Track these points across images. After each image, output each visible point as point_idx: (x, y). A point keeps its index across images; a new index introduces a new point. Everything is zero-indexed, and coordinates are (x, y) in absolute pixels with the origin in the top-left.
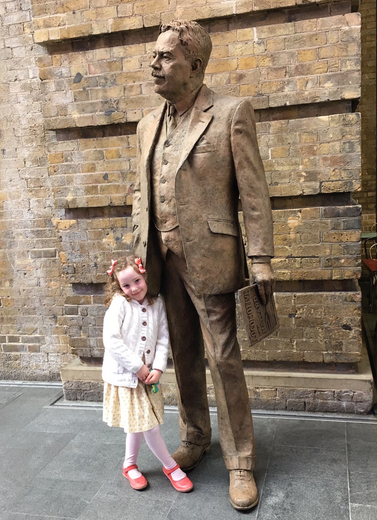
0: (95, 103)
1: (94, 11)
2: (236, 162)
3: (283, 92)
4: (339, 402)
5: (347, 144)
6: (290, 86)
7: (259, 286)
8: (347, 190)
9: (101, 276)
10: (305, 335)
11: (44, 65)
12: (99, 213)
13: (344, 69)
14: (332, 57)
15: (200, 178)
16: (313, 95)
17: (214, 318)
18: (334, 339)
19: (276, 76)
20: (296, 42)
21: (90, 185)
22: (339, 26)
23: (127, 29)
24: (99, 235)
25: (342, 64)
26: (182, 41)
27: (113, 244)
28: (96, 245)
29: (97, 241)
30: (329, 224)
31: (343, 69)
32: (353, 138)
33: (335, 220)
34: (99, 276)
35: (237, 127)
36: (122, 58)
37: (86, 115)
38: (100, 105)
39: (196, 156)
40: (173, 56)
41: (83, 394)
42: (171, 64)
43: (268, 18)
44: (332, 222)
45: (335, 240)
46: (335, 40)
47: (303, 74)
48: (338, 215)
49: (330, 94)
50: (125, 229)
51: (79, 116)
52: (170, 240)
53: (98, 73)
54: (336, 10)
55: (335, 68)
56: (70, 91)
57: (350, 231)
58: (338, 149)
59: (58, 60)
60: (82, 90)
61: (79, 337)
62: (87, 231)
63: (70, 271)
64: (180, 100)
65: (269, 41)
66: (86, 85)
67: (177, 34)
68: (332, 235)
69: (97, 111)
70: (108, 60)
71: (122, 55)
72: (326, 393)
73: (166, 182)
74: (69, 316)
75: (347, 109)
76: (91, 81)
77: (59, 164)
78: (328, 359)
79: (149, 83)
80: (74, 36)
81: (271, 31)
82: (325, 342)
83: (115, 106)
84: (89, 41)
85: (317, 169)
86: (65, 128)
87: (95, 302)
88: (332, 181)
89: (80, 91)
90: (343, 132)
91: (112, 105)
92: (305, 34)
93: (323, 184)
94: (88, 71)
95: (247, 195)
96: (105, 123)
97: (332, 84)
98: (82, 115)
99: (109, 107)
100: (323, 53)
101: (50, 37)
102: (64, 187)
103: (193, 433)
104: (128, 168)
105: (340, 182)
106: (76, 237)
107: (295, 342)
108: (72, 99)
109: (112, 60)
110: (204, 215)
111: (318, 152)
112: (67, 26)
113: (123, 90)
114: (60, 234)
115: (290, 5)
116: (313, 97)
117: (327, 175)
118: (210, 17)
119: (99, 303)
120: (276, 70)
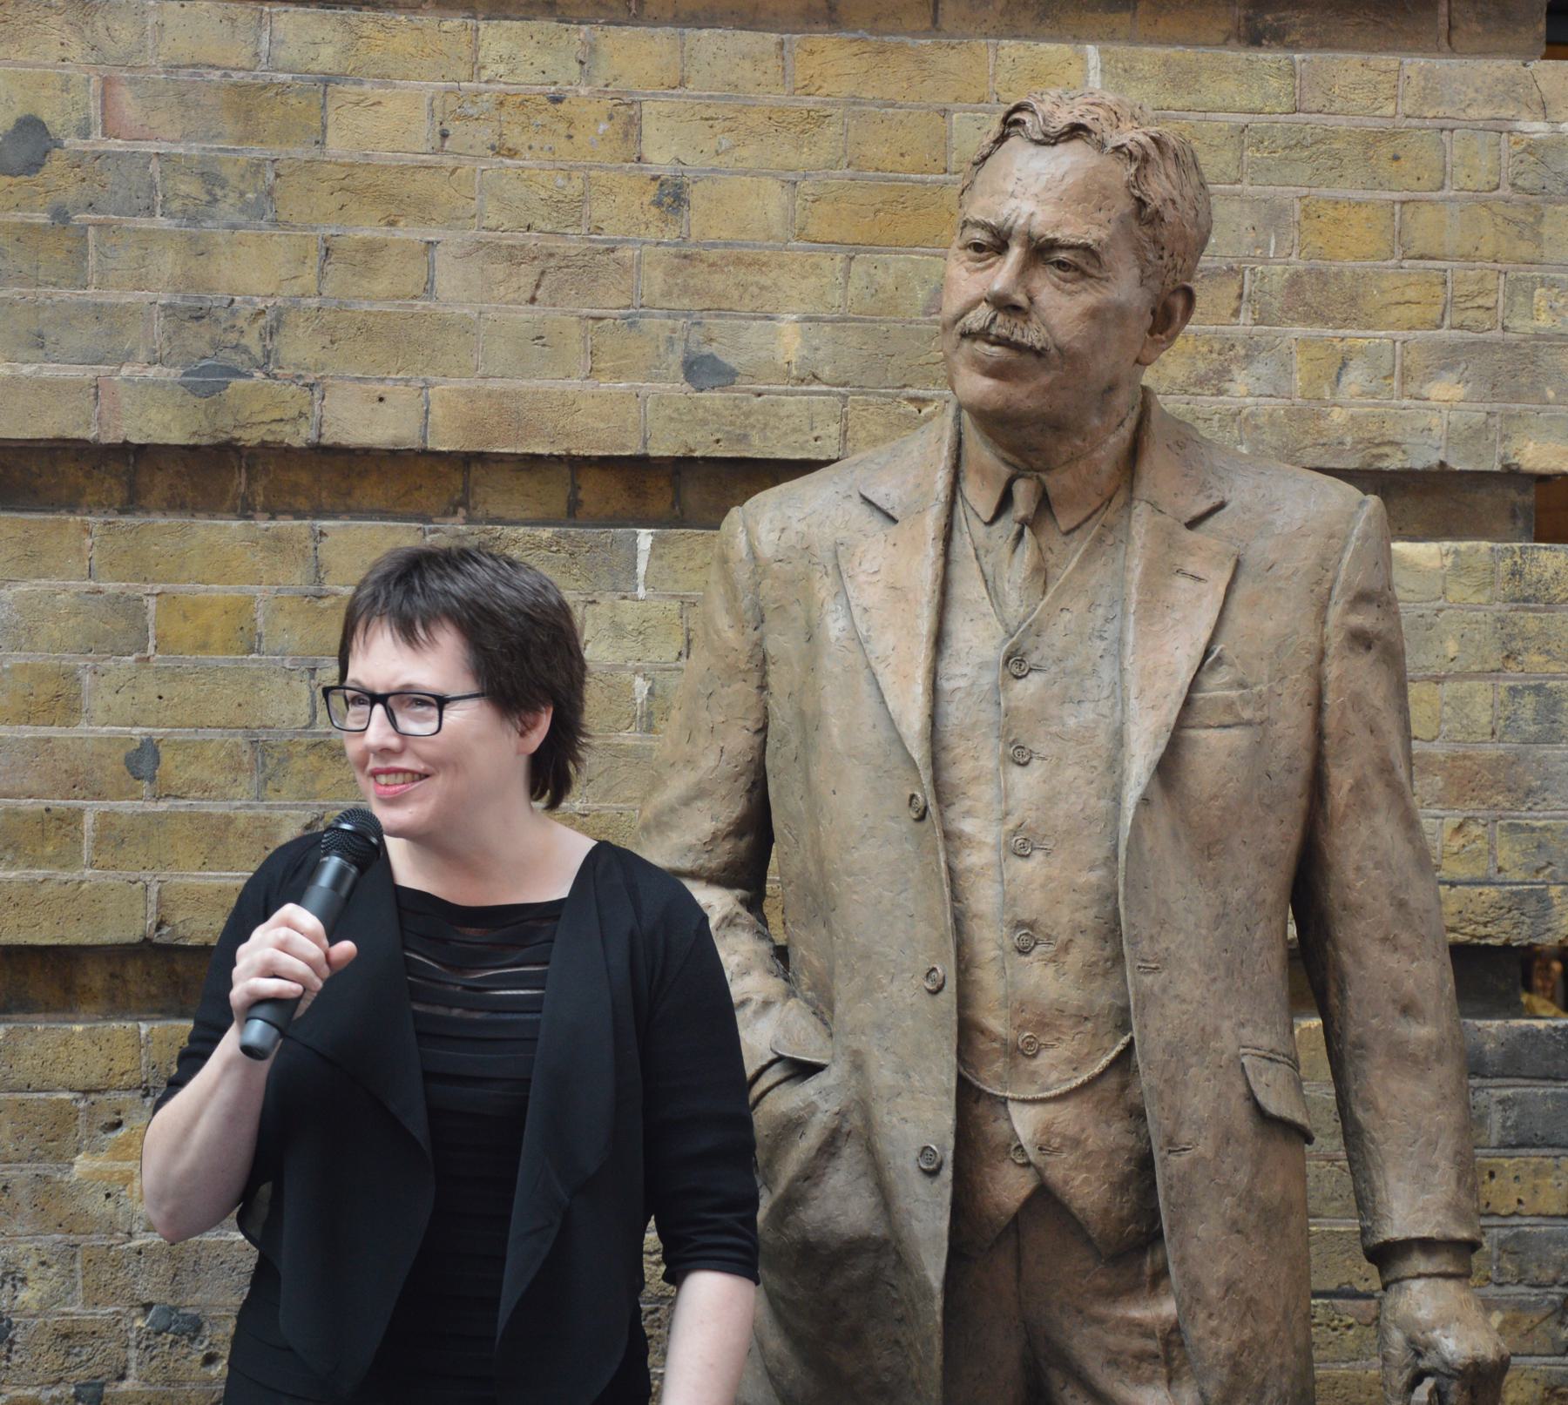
0: (125, 308)
2: (1341, 780)
3: (1220, 392)
5: (1529, 700)
6: (1260, 369)
8: (1521, 935)
13: (1522, 325)
14: (1466, 257)
15: (1208, 847)
20: (1295, 154)
21: (26, 804)
22: (1504, 113)
25: (1510, 298)
26: (1141, 203)
29: (30, 1169)
31: (1516, 323)
32: (1553, 668)
36: (327, 80)
37: (50, 371)
38: (159, 324)
46: (1481, 179)
52: (1056, 1142)
53: (169, 138)
55: (1480, 314)
57: (1534, 1156)
58: (1485, 718)
60: (41, 218)
64: (1072, 460)
69: (129, 357)
70: (236, 76)
71: (327, 59)
73: (1038, 856)
75: (1514, 516)
79: (480, 245)
83: (252, 341)
88: (1453, 884)
89: (31, 227)
90: (1511, 637)
91: (232, 337)
94: (95, 113)
95: (1385, 940)
96: (176, 437)
97: (1460, 391)
98: (27, 370)
99: (216, 345)
100: (1424, 228)
104: (304, 719)
105: (1491, 893)
110: (1226, 1025)
113: (314, 260)
116: (1371, 443)
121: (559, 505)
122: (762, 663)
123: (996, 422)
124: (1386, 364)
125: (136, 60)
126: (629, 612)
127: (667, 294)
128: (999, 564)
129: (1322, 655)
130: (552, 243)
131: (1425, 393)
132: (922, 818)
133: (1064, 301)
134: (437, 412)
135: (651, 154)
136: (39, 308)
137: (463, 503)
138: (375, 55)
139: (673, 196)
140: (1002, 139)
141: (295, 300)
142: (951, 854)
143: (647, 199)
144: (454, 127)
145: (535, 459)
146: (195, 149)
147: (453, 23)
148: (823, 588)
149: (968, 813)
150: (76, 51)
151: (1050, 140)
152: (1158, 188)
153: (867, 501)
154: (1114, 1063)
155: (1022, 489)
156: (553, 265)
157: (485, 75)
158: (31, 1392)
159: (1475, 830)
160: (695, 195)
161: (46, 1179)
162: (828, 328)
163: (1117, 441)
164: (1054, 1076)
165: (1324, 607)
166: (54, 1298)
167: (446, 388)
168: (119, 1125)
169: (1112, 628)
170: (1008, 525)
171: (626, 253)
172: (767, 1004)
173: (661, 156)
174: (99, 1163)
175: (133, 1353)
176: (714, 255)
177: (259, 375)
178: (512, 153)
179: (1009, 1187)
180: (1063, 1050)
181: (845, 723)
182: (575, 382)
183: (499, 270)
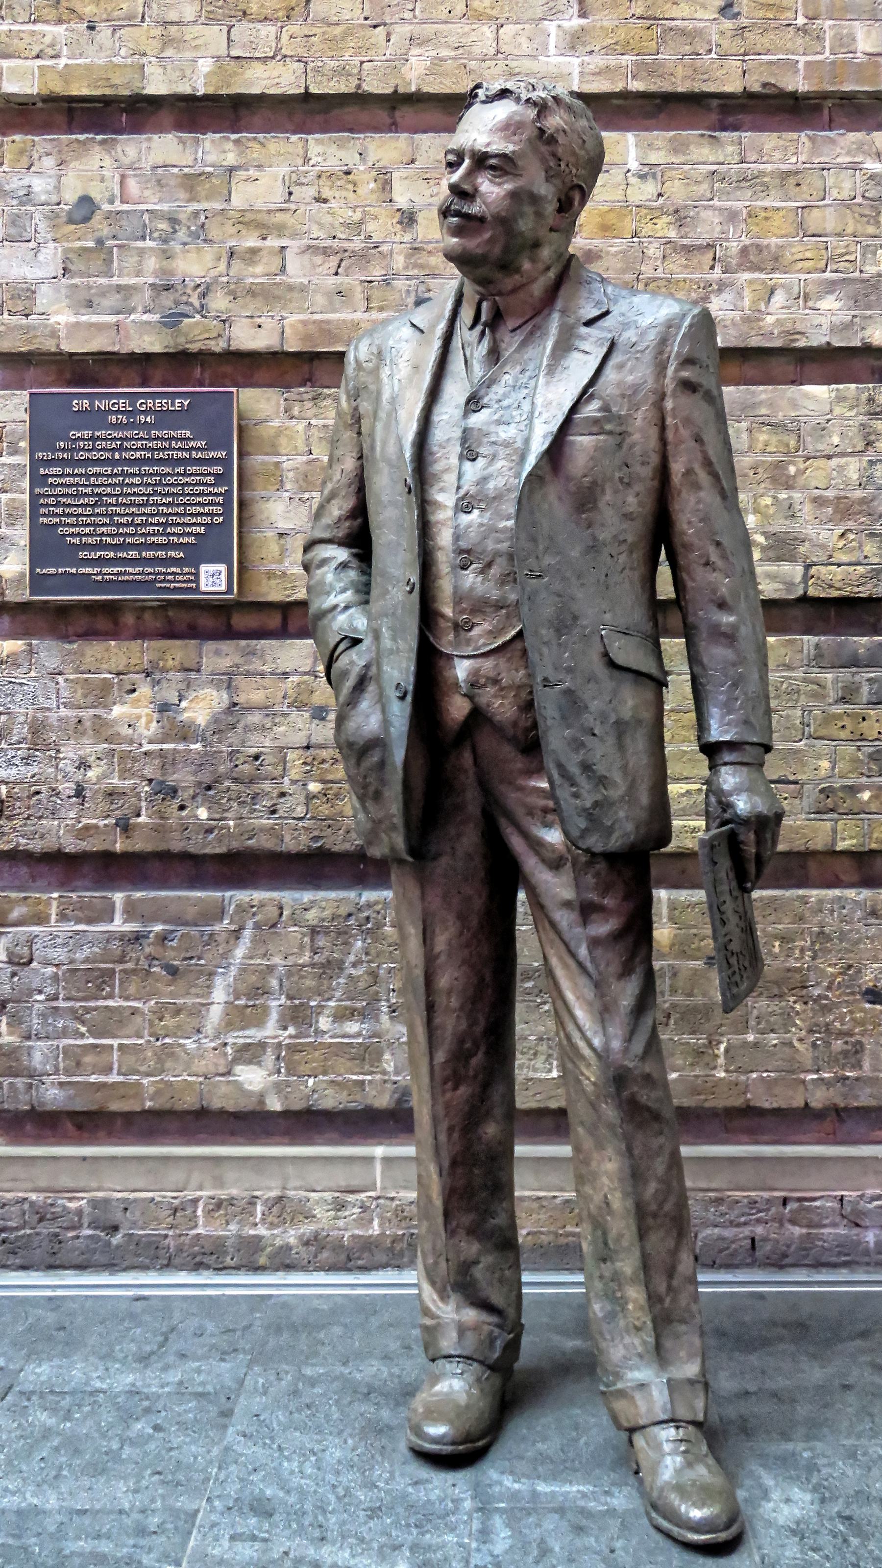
1: (157, 31)
2: (677, 468)
4: (856, 1231)
7: (741, 830)
9: (96, 827)
10: (752, 1023)
12: (102, 623)
14: (838, 235)
16: (789, 326)
17: (603, 928)
18: (841, 1034)
19: (686, 266)
20: (743, 184)
22: (856, 160)
23: (256, 90)
24: (102, 695)
25: (863, 255)
26: (542, 131)
27: (149, 722)
28: (88, 724)
29: (92, 712)
30: (829, 685)
33: (845, 674)
34: (87, 828)
35: (685, 374)
36: (231, 170)
37: (95, 319)
38: (148, 293)
39: (573, 443)
40: (515, 164)
42: (508, 186)
43: (662, 116)
44: (836, 681)
45: (843, 734)
46: (845, 195)
47: (761, 270)
48: (854, 662)
49: (833, 329)
50: (193, 675)
51: (73, 319)
52: (482, 681)
54: (845, 120)
55: (847, 264)
56: (52, 245)
58: (855, 476)
60: (91, 244)
62: (60, 679)
65: (668, 174)
67: (532, 113)
68: (839, 717)
70: (186, 170)
71: (231, 159)
72: (817, 1203)
73: (476, 512)
75: (873, 373)
76: (124, 223)
78: (818, 1099)
79: (309, 247)
80: (85, 92)
81: (678, 148)
82: (814, 1045)
83: (195, 300)
84: (124, 110)
85: (795, 527)
86: (20, 354)
89: (86, 249)
90: (869, 434)
91: (185, 298)
92: (769, 167)
93: (813, 570)
94: (117, 191)
96: (157, 348)
97: (838, 305)
98: (84, 318)
99: (177, 303)
100: (814, 220)
103: (476, 1328)
106: (19, 697)
107: (722, 1047)
109: (197, 170)
111: (801, 481)
112: (63, 61)
115: (728, 89)
117: (823, 547)
119: (78, 921)
120: (688, 250)
124: (796, 289)
127: (406, 268)
129: (663, 397)
130: (346, 245)
131: (817, 306)
133: (496, 190)
134: (288, 331)
135: (395, 197)
136: (90, 288)
137: (310, 380)
143: (395, 221)
147: (294, 138)
149: (442, 490)
150: (108, 162)
153: (413, 325)
157: (311, 163)
159: (851, 536)
160: (420, 217)
164: (481, 641)
166: (105, 776)
167: (292, 318)
168: (134, 691)
169: (532, 382)
171: (384, 248)
173: (402, 200)
175: (143, 804)
176: (430, 247)
177: (198, 317)
178: (325, 201)
179: (458, 708)
180: (486, 626)
183: (318, 259)
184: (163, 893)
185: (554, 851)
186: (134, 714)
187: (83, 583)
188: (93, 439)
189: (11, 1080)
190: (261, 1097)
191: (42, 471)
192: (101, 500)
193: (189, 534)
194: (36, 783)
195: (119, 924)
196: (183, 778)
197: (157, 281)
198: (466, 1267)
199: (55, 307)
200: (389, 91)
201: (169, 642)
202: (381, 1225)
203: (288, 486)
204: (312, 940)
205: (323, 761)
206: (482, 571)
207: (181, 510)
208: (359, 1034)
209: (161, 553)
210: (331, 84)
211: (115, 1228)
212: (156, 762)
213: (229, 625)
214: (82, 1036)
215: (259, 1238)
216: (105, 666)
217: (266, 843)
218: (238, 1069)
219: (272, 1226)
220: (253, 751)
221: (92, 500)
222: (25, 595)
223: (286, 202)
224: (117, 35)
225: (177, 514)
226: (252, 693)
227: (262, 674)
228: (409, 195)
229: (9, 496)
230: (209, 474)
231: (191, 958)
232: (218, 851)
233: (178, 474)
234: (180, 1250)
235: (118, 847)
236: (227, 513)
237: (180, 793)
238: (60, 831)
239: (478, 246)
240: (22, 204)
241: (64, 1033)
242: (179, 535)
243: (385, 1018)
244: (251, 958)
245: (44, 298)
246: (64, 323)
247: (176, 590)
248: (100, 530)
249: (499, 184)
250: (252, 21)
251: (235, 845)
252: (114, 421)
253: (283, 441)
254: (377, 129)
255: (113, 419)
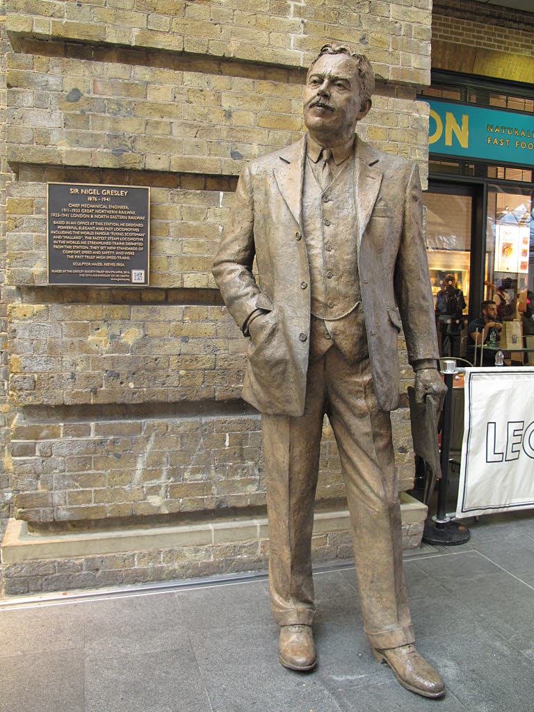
2: (409, 235)
9: (82, 392)
11: (18, 66)
22: (410, 111)
23: (160, 47)
24: (83, 330)
25: (411, 151)
26: (360, 70)
27: (106, 344)
34: (77, 393)
35: (414, 192)
36: (148, 83)
37: (80, 149)
40: (350, 86)
41: (40, 582)
46: (405, 125)
51: (69, 149)
59: (43, 64)
60: (78, 112)
61: (34, 492)
62: (63, 323)
63: (26, 386)
66: (86, 107)
69: (99, 146)
70: (126, 81)
71: (147, 78)
73: (333, 251)
74: (18, 458)
77: (25, 217)
79: (183, 123)
80: (76, 37)
86: (42, 164)
87: (66, 434)
91: (124, 143)
94: (91, 87)
96: (110, 166)
98: (74, 149)
99: (120, 145)
100: (394, 134)
101: (34, 28)
102: (29, 252)
106: (42, 332)
108: (60, 123)
109: (131, 81)
112: (65, 21)
114: (13, 326)
118: (272, 61)
121: (202, 186)
122: (252, 203)
123: (317, 131)
125: (102, 76)
126: (218, 211)
128: (319, 176)
129: (405, 201)
132: (300, 239)
134: (173, 162)
135: (223, 105)
138: (159, 78)
139: (228, 115)
140: (320, 55)
141: (139, 134)
142: (308, 250)
144: (177, 96)
145: (197, 175)
146: (116, 98)
148: (270, 180)
149: (312, 239)
150: (87, 73)
151: (335, 52)
152: (364, 67)
154: (354, 310)
155: (325, 153)
156: (201, 129)
157: (185, 84)
158: (80, 390)
160: (233, 115)
161: (82, 341)
162: (264, 147)
163: (350, 143)
164: (337, 313)
165: (406, 189)
167: (175, 156)
168: (99, 329)
169: (351, 190)
170: (322, 163)
172: (254, 294)
173: (226, 106)
174: (95, 338)
175: (104, 381)
176: (238, 129)
178: (191, 103)
179: (325, 345)
180: (340, 306)
181: (279, 215)
182: (205, 157)
183: (188, 130)
184: (113, 422)
185: (361, 410)
186: (98, 340)
187: (75, 277)
188: (80, 208)
189: (44, 509)
190: (159, 508)
191: (55, 222)
192: (84, 238)
193: (127, 255)
194: (52, 373)
195: (93, 436)
196: (121, 369)
197: (111, 133)
198: (299, 587)
199: (60, 142)
200: (221, 55)
201: (115, 306)
202: (214, 557)
203: (172, 234)
204: (181, 440)
205: (187, 361)
206: (338, 280)
207: (123, 243)
208: (202, 479)
209: (113, 264)
210: (195, 48)
211: (97, 570)
212: (110, 362)
213: (141, 298)
214: (77, 487)
215: (163, 567)
216: (85, 317)
217: (161, 398)
218: (149, 497)
219: (168, 562)
220: (154, 357)
221: (80, 238)
222: (46, 283)
223: (173, 101)
224: (92, 11)
225: (121, 246)
226: (154, 330)
227: (159, 321)
228: (229, 104)
229: (36, 234)
230: (137, 227)
231: (127, 450)
232: (139, 402)
233: (122, 226)
234: (127, 576)
235: (92, 402)
236: (145, 246)
237: (120, 376)
238: (64, 395)
239: (330, 123)
240: (43, 89)
241: (68, 486)
242: (122, 256)
243: (213, 471)
244: (154, 449)
245: (55, 137)
246: (65, 150)
247: (120, 282)
248: (83, 252)
249: (342, 94)
250: (159, 13)
251: (147, 399)
252: (91, 199)
253: (170, 213)
254: (212, 73)
255: (90, 199)
